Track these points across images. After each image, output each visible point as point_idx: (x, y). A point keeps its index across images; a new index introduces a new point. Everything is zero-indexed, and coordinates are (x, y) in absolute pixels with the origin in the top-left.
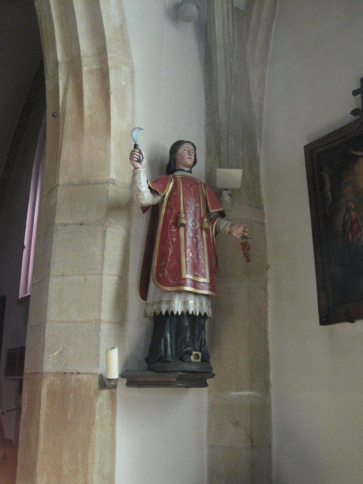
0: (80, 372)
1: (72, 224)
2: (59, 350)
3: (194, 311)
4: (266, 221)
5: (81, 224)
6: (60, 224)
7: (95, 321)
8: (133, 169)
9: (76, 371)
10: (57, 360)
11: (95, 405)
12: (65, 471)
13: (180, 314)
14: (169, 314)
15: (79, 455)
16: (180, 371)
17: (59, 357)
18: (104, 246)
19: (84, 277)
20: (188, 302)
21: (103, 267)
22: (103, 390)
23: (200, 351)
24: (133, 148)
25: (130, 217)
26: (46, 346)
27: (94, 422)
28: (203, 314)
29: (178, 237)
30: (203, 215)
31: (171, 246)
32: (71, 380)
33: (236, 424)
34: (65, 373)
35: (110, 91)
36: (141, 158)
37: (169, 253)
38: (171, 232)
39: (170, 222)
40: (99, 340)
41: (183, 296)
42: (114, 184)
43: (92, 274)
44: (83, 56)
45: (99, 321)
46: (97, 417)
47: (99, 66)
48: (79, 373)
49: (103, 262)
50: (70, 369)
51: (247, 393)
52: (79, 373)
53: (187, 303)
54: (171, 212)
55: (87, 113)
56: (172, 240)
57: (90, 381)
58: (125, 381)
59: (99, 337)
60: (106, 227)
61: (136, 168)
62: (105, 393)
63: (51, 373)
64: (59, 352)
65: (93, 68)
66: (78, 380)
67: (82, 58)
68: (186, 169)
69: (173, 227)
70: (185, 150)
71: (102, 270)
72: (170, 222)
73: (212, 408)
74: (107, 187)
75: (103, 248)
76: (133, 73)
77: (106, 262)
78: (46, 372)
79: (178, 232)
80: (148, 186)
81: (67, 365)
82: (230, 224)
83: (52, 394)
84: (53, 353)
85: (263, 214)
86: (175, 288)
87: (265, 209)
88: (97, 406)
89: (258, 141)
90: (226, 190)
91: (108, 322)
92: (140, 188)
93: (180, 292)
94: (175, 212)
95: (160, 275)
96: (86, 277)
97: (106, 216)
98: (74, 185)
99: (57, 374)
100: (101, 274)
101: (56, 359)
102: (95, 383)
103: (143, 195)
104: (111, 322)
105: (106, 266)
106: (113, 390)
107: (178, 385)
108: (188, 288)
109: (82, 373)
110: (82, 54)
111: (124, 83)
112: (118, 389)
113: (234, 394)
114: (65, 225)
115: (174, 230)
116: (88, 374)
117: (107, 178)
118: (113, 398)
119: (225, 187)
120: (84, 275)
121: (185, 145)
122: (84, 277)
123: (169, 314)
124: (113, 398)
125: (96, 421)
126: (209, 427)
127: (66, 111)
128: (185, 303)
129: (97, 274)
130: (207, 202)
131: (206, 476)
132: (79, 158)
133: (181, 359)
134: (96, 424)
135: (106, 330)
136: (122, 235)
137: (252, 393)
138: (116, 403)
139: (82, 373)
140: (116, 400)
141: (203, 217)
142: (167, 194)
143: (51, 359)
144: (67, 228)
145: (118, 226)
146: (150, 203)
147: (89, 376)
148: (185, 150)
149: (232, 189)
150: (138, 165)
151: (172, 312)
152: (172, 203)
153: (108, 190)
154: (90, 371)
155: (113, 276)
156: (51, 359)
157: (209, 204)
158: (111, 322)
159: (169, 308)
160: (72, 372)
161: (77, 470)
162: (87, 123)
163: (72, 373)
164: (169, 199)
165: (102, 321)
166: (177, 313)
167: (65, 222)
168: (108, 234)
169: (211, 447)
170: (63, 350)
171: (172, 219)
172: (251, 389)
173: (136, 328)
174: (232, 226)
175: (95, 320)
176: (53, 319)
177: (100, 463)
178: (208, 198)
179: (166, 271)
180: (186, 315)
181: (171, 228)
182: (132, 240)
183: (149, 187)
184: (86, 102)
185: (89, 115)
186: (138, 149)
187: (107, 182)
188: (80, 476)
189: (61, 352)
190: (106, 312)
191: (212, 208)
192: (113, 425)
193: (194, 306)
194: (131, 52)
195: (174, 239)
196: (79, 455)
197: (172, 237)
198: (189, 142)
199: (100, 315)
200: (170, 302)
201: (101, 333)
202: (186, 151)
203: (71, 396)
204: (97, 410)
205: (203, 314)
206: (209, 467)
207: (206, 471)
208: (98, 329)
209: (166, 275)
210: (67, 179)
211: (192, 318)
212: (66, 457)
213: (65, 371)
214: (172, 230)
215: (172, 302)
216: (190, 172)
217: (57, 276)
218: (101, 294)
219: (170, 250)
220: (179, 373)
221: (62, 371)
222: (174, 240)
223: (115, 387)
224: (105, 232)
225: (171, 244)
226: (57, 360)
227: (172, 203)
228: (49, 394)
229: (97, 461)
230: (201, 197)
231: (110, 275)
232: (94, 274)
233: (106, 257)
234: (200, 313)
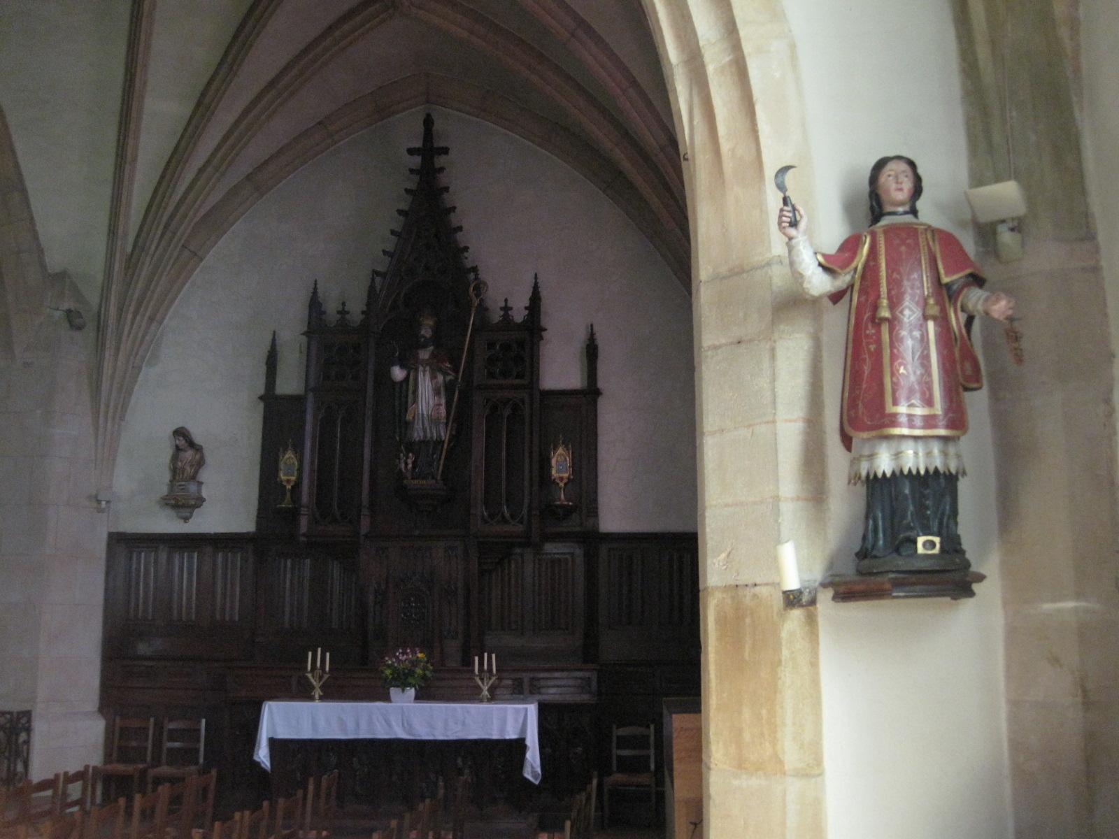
0: (758, 582)
1: (726, 345)
2: (726, 549)
3: (929, 466)
4: (1104, 263)
5: (739, 342)
6: (709, 348)
7: (771, 500)
8: (787, 240)
9: (750, 582)
10: (725, 567)
11: (780, 633)
12: (747, 736)
13: (922, 472)
14: (871, 477)
15: (764, 712)
16: (893, 572)
17: (727, 562)
18: (774, 374)
19: (751, 430)
20: (905, 452)
21: (775, 409)
22: (791, 609)
23: (939, 534)
24: (781, 204)
25: (817, 318)
26: (708, 545)
27: (780, 661)
28: (931, 470)
29: (879, 342)
30: (928, 291)
31: (868, 360)
32: (745, 596)
33: (1055, 661)
34: (737, 586)
35: (754, 99)
36: (798, 218)
37: (864, 373)
38: (867, 336)
39: (865, 318)
40: (779, 530)
41: (894, 444)
42: (782, 264)
43: (760, 423)
44: (703, 47)
45: (777, 499)
46: (785, 653)
47: (731, 57)
48: (755, 585)
49: (774, 403)
50: (742, 580)
51: (1070, 604)
52: (755, 585)
53: (901, 455)
54: (867, 300)
55: (725, 146)
56: (869, 350)
57: (771, 595)
58: (830, 593)
59: (779, 525)
60: (775, 342)
61: (790, 239)
62: (797, 614)
63: (717, 588)
64: (727, 553)
65: (723, 62)
66: (755, 595)
67: (703, 51)
68: (901, 209)
69: (870, 326)
70: (889, 176)
71: (775, 414)
72: (865, 318)
73: (1013, 635)
74: (769, 271)
75: (774, 379)
76: (793, 47)
77: (779, 401)
78: (712, 587)
79: (879, 333)
80: (817, 263)
81: (738, 574)
82: (984, 297)
83: (722, 621)
84: (719, 556)
85: (1097, 250)
86: (874, 433)
87: (1101, 238)
88: (784, 635)
89: (1075, 99)
90: (1003, 221)
91: (792, 499)
92: (802, 272)
93: (888, 438)
94: (871, 299)
95: (852, 413)
96: (753, 430)
97: (773, 323)
98: (724, 278)
99: (726, 588)
100: (774, 422)
101: (724, 565)
102: (778, 601)
103: (810, 282)
104: (798, 498)
105: (780, 407)
106: (811, 608)
107: (895, 594)
108: (905, 431)
109: (760, 585)
110: (701, 43)
111: (777, 75)
112: (820, 606)
113: (1047, 606)
114: (716, 348)
115: (871, 331)
116: (767, 584)
117: (768, 255)
118: (811, 621)
119: (996, 218)
120: (750, 426)
121: (892, 167)
122: (751, 430)
123: (871, 477)
124: (811, 621)
125: (783, 658)
126: (1008, 668)
127: (696, 150)
128: (897, 455)
129: (768, 422)
130: (936, 265)
131: (1006, 755)
132: (724, 230)
133: (897, 550)
134: (783, 663)
135: (791, 512)
136: (806, 348)
137: (1083, 604)
138: (818, 630)
139: (760, 585)
140: (817, 625)
141: (928, 295)
142: (860, 267)
143: (717, 566)
144: (719, 351)
145: (798, 336)
146: (830, 291)
147: (769, 587)
148: (889, 176)
149: (1013, 219)
150: (792, 232)
151: (875, 475)
152: (867, 283)
153: (770, 277)
154: (770, 581)
155: (795, 421)
156: (717, 566)
157: (941, 267)
158: (798, 498)
159: (871, 467)
160: (747, 583)
161: (762, 734)
162: (728, 165)
163: (746, 585)
164: (863, 277)
165: (782, 499)
166: (884, 474)
167: (717, 343)
168: (780, 353)
169: (1014, 704)
170: (732, 550)
171: (867, 311)
172: (1079, 595)
173: (843, 505)
174: (987, 300)
175: (771, 497)
176: (714, 503)
177: (794, 724)
178: (939, 256)
179: (860, 405)
180: (898, 477)
181: (866, 328)
182: (825, 355)
183: (820, 265)
184: (722, 129)
185: (729, 150)
186: (789, 204)
187: (769, 264)
188: (767, 744)
189: (729, 553)
190: (789, 482)
191: (947, 274)
192: (814, 664)
193: (914, 458)
194: (783, 11)
195: (872, 347)
196: (764, 712)
197: (868, 344)
198: (899, 158)
199: (778, 488)
200: (871, 457)
201: (781, 518)
202: (891, 178)
203: (748, 620)
204: (784, 642)
205: (931, 470)
206: (1011, 740)
207: (1005, 745)
208: (777, 512)
209: (860, 413)
210: (711, 270)
211: (917, 480)
212: (747, 714)
213: (738, 583)
214: (868, 332)
215: (875, 457)
216: (914, 212)
217: (713, 433)
218: (776, 454)
219: (866, 368)
220: (892, 575)
221: (733, 583)
222: (872, 349)
223: (813, 602)
224: (773, 350)
225: (867, 356)
226: (725, 567)
227: (867, 283)
228: (717, 622)
229: (789, 721)
230: (923, 258)
231: (790, 421)
232: (765, 423)
233: (780, 392)
234: (927, 471)
